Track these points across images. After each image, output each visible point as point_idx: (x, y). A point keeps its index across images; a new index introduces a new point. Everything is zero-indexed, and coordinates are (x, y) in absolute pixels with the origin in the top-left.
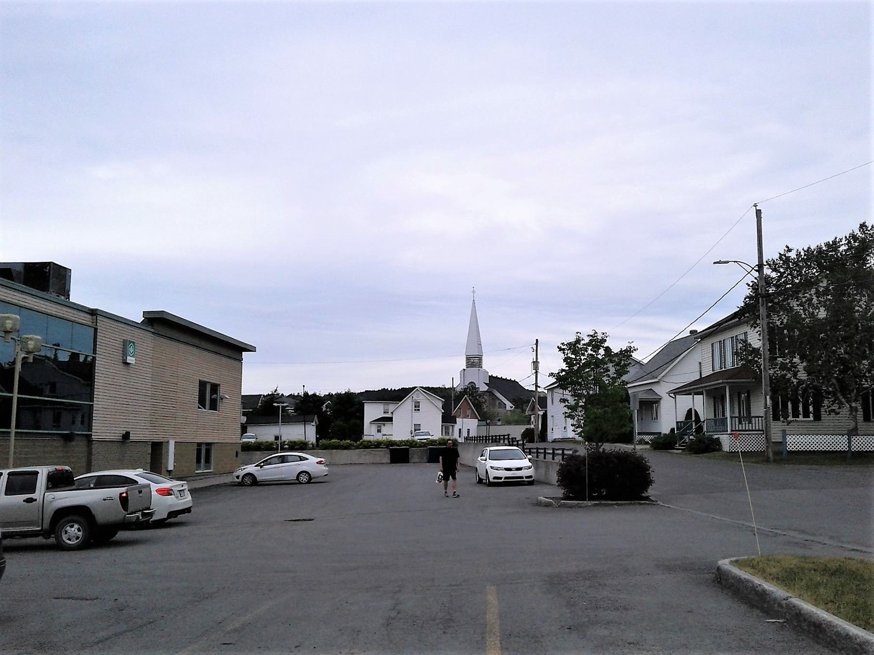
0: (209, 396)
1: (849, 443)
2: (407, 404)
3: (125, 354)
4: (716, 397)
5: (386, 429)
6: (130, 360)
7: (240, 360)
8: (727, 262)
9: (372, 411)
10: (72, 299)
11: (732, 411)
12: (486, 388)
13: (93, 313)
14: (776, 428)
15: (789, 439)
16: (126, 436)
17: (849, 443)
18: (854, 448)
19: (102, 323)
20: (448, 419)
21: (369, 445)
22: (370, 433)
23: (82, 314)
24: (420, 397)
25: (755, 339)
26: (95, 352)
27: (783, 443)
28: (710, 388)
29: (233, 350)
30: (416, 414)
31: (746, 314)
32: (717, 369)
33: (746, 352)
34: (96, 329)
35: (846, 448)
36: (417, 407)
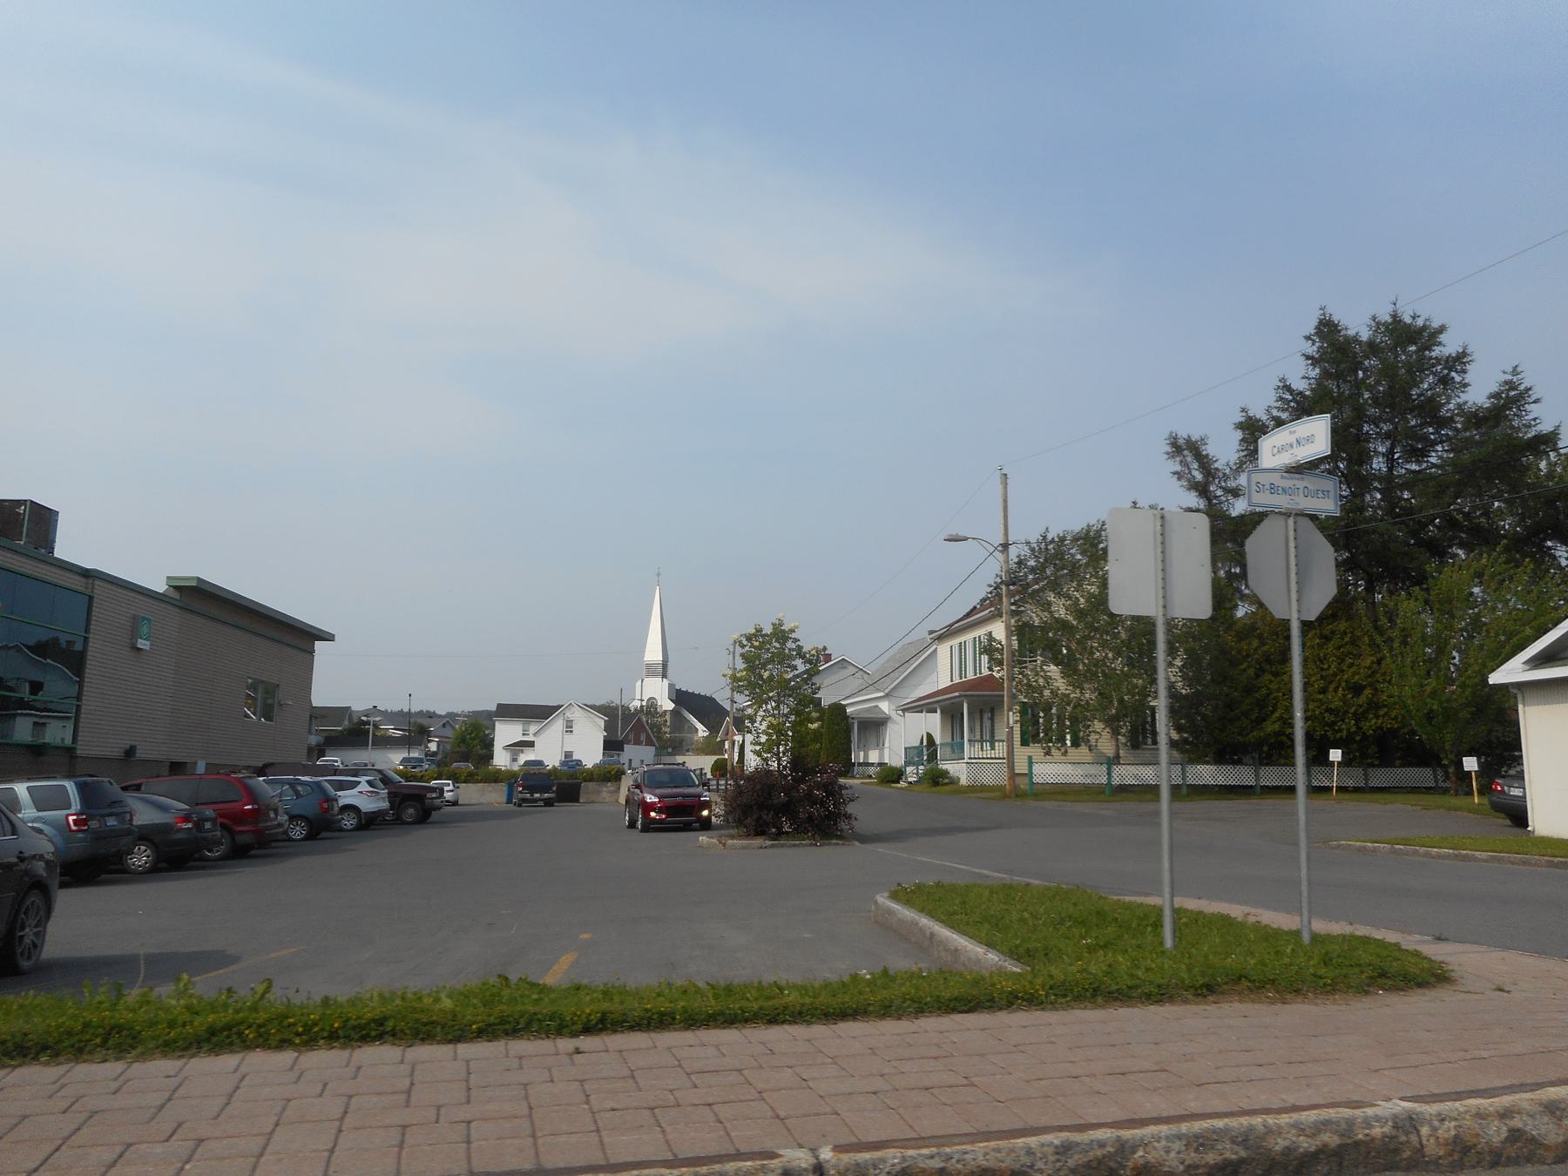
0: (267, 700)
1: (1109, 774)
2: (557, 725)
3: (134, 634)
4: (952, 715)
5: (527, 756)
6: (142, 644)
7: (312, 652)
8: (966, 539)
9: (506, 733)
10: (60, 552)
11: (972, 730)
12: (670, 706)
13: (87, 574)
14: (1021, 753)
15: (1036, 768)
16: (130, 752)
17: (1109, 774)
18: (1116, 781)
19: (100, 589)
20: (611, 745)
21: (496, 777)
22: (501, 759)
23: (70, 575)
24: (576, 714)
25: (998, 630)
26: (87, 630)
27: (1030, 775)
28: (949, 706)
29: (301, 638)
30: (568, 737)
31: (989, 607)
32: (957, 680)
33: (989, 648)
34: (91, 598)
35: (1104, 780)
36: (569, 728)
